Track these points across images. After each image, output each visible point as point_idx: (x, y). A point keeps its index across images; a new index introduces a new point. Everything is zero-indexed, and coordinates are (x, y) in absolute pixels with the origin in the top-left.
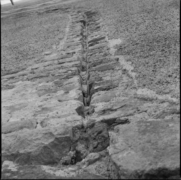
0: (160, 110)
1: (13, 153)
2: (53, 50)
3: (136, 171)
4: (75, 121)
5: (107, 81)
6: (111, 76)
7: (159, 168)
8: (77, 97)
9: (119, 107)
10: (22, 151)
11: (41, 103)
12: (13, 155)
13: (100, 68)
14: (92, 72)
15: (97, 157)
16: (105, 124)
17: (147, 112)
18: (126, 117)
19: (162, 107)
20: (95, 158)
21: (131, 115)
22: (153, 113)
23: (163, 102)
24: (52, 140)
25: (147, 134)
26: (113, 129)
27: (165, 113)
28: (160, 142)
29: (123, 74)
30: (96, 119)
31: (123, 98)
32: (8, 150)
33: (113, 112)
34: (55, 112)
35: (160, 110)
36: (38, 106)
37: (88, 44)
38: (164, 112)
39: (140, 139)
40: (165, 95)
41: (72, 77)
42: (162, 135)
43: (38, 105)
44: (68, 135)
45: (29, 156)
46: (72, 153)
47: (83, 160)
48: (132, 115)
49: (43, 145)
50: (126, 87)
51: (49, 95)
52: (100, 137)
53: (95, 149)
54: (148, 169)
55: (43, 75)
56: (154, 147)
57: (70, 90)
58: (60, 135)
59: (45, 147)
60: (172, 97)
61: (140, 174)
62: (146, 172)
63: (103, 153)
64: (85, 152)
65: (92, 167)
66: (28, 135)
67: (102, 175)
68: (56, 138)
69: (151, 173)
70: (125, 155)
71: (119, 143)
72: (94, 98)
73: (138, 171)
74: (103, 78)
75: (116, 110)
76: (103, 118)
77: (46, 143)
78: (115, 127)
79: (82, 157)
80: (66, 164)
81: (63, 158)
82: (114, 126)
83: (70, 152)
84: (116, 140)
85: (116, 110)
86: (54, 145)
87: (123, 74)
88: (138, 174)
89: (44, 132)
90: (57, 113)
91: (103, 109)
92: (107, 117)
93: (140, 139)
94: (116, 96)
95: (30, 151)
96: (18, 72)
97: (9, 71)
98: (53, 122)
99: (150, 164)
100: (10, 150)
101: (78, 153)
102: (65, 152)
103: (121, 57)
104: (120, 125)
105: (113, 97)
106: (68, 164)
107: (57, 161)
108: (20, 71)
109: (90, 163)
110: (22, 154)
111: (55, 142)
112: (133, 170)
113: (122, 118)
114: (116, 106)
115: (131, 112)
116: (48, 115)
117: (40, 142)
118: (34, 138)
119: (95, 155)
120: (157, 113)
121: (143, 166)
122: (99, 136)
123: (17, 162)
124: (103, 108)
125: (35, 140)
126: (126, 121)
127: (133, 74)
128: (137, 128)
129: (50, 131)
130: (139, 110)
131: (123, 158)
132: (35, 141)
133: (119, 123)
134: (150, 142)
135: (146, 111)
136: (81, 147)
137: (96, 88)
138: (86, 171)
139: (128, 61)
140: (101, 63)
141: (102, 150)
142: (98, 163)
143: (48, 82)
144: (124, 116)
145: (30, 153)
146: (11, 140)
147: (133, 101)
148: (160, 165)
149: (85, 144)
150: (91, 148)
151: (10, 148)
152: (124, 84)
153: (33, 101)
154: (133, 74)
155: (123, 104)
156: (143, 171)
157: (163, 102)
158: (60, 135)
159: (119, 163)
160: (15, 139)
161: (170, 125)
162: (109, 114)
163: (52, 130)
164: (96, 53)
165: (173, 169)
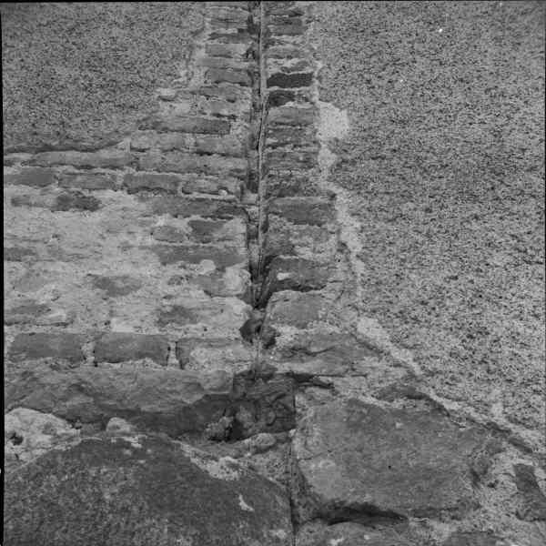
0: (388, 381)
1: (130, 407)
2: (178, 83)
3: (333, 501)
4: (240, 361)
5: (304, 260)
6: (314, 251)
7: (366, 503)
8: (240, 292)
9: (321, 349)
10: (145, 408)
11: (170, 290)
12: (128, 410)
13: (295, 207)
14: (276, 217)
15: (271, 444)
16: (291, 380)
17: (368, 377)
18: (330, 379)
19: (393, 376)
20: (269, 444)
21: (339, 375)
22: (377, 385)
23: (398, 365)
24: (198, 396)
25: (360, 433)
26: (303, 391)
27: (396, 391)
28: (376, 457)
29: (338, 250)
30: (278, 366)
31: (332, 329)
32: (120, 401)
33: (310, 357)
34: (200, 325)
35: (388, 381)
36: (163, 295)
37: (269, 86)
38: (393, 388)
39: (346, 439)
40: (404, 350)
41: (230, 216)
42: (382, 442)
43: (164, 293)
44: (226, 392)
45: (156, 419)
46: (227, 420)
47: (247, 441)
48: (341, 376)
49: (183, 405)
50: (339, 294)
51: (184, 267)
52: (280, 407)
53: (269, 428)
54: (350, 501)
55: (162, 186)
56: (366, 463)
57: (229, 265)
58: (214, 390)
59: (186, 408)
60: (414, 360)
61: (338, 505)
62: (346, 505)
63: (281, 436)
64: (250, 427)
65: (261, 461)
66: (158, 380)
67: (277, 480)
68: (207, 396)
69: (353, 507)
70: (320, 465)
71: (314, 439)
72: (277, 306)
73: (337, 502)
74: (298, 249)
75: (314, 355)
76: (290, 367)
77: (189, 402)
78: (310, 389)
79: (244, 433)
80: (215, 439)
81: (209, 426)
82: (306, 386)
83: (225, 418)
84: (310, 431)
85: (314, 355)
86: (199, 405)
87: (338, 250)
88: (334, 505)
89: (186, 380)
90: (205, 330)
91: (292, 345)
92: (300, 368)
93: (346, 439)
94: (318, 319)
95: (159, 410)
96: (97, 149)
97: (76, 141)
98: (200, 354)
99: (355, 493)
100: (126, 402)
101: (236, 423)
102: (214, 415)
103: (343, 197)
104: (317, 388)
105: (314, 319)
106: (220, 441)
107: (200, 429)
108: (102, 148)
109: (259, 451)
110: (144, 412)
111: (204, 401)
112: (329, 498)
113: (323, 379)
114: (315, 345)
115: (341, 369)
116: (188, 329)
117: (179, 398)
118: (168, 388)
119: (264, 438)
120: (383, 386)
121: (345, 494)
122: (280, 403)
123: (134, 423)
124: (291, 342)
125: (171, 392)
126: (329, 385)
127: (360, 267)
128: (345, 414)
129: (198, 381)
130: (354, 370)
131: (317, 472)
132: (170, 395)
133: (315, 385)
134: (361, 451)
135: (365, 376)
136: (245, 416)
137: (281, 276)
138: (253, 469)
139: (353, 215)
140: (296, 190)
141: (280, 432)
142: (271, 454)
143: (176, 217)
144: (328, 376)
145: (161, 413)
146: (126, 382)
147: (347, 344)
148: (368, 498)
149: (253, 410)
150: (262, 423)
151: (125, 398)
152: (338, 286)
153: (151, 276)
154: (360, 267)
155: (329, 344)
156: (342, 503)
157: (398, 365)
158: (214, 390)
159: (310, 480)
160: (133, 383)
161: (398, 425)
162: (303, 361)
163: (200, 378)
164: (287, 143)
165: (384, 510)
